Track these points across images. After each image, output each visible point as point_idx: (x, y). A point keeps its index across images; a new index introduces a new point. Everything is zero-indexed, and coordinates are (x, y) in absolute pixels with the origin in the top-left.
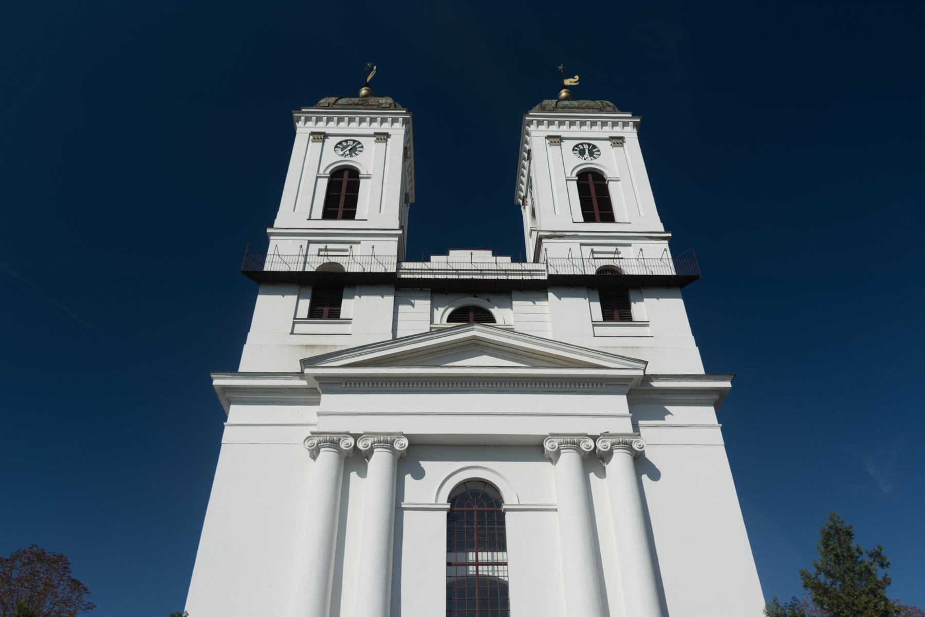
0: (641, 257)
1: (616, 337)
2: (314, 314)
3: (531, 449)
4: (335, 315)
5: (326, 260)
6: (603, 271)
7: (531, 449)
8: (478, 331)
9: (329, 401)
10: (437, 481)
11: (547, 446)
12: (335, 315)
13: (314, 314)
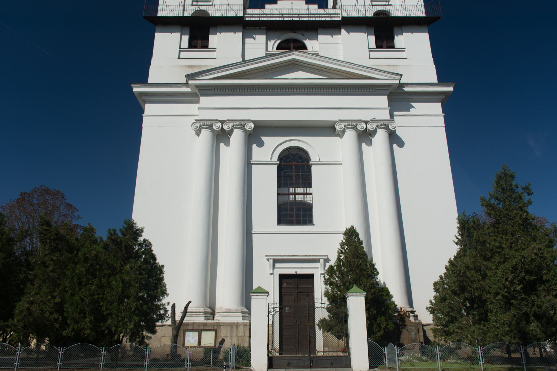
0: (165, 4)
1: (384, 59)
2: (192, 45)
3: (328, 129)
4: (205, 46)
5: (197, 8)
6: (378, 14)
7: (328, 129)
8: (296, 55)
9: (205, 101)
10: (271, 148)
11: (337, 127)
12: (205, 46)
13: (192, 45)
